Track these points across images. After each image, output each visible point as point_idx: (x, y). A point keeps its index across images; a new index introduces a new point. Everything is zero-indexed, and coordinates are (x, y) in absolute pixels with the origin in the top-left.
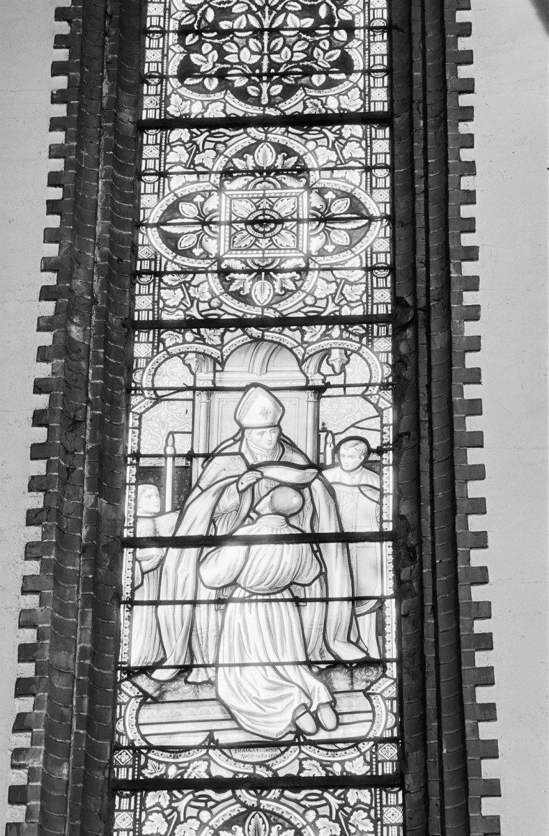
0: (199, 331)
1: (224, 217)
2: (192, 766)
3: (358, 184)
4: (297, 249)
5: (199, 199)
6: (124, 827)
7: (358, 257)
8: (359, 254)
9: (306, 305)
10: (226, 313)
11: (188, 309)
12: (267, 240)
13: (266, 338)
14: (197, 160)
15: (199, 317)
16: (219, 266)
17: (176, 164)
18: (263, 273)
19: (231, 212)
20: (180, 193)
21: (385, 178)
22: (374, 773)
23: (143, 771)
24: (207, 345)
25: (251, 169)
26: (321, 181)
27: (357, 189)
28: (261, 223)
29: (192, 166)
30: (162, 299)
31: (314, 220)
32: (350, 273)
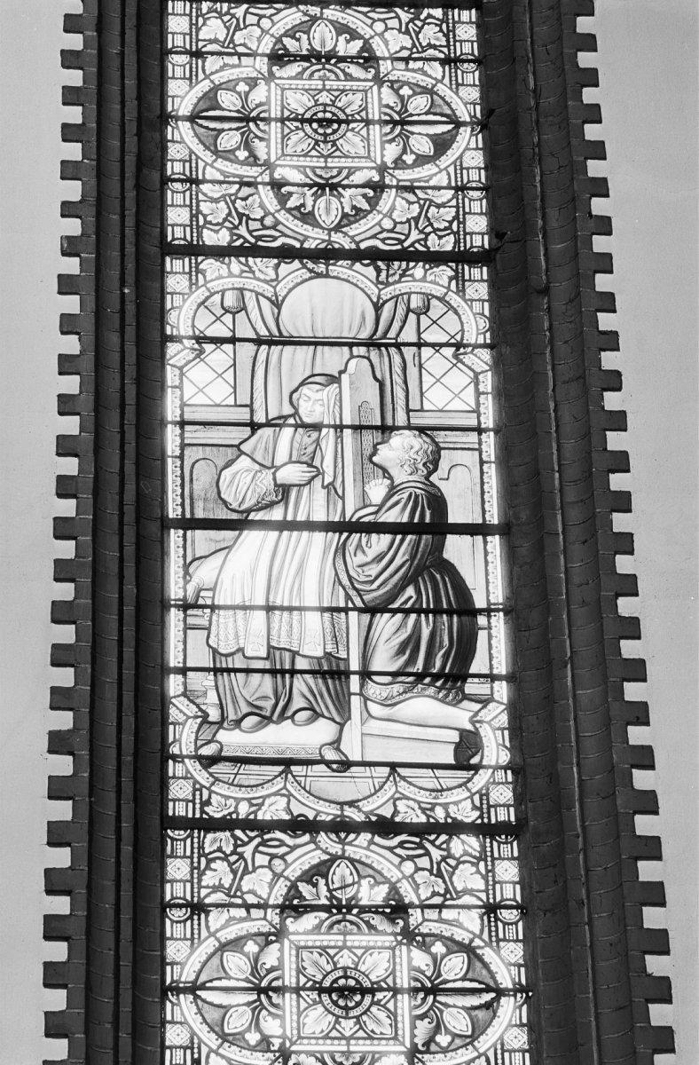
0: (247, 261)
1: (275, 112)
2: (268, 802)
3: (440, 77)
4: (368, 157)
5: (242, 87)
6: (178, 878)
7: (444, 172)
8: (446, 169)
9: (383, 230)
10: (365, 14)
11: (236, 227)
12: (321, 101)
13: (330, 273)
14: (239, 38)
15: (397, 10)
16: (271, 175)
17: (211, 41)
18: (327, 189)
19: (283, 107)
20: (217, 78)
21: (473, 72)
22: (486, 820)
23: (206, 809)
24: (259, 279)
25: (305, 52)
26: (394, 72)
27: (439, 85)
28: (342, 991)
29: (422, 202)
30: (202, 214)
31: (387, 123)
32: (437, 193)
